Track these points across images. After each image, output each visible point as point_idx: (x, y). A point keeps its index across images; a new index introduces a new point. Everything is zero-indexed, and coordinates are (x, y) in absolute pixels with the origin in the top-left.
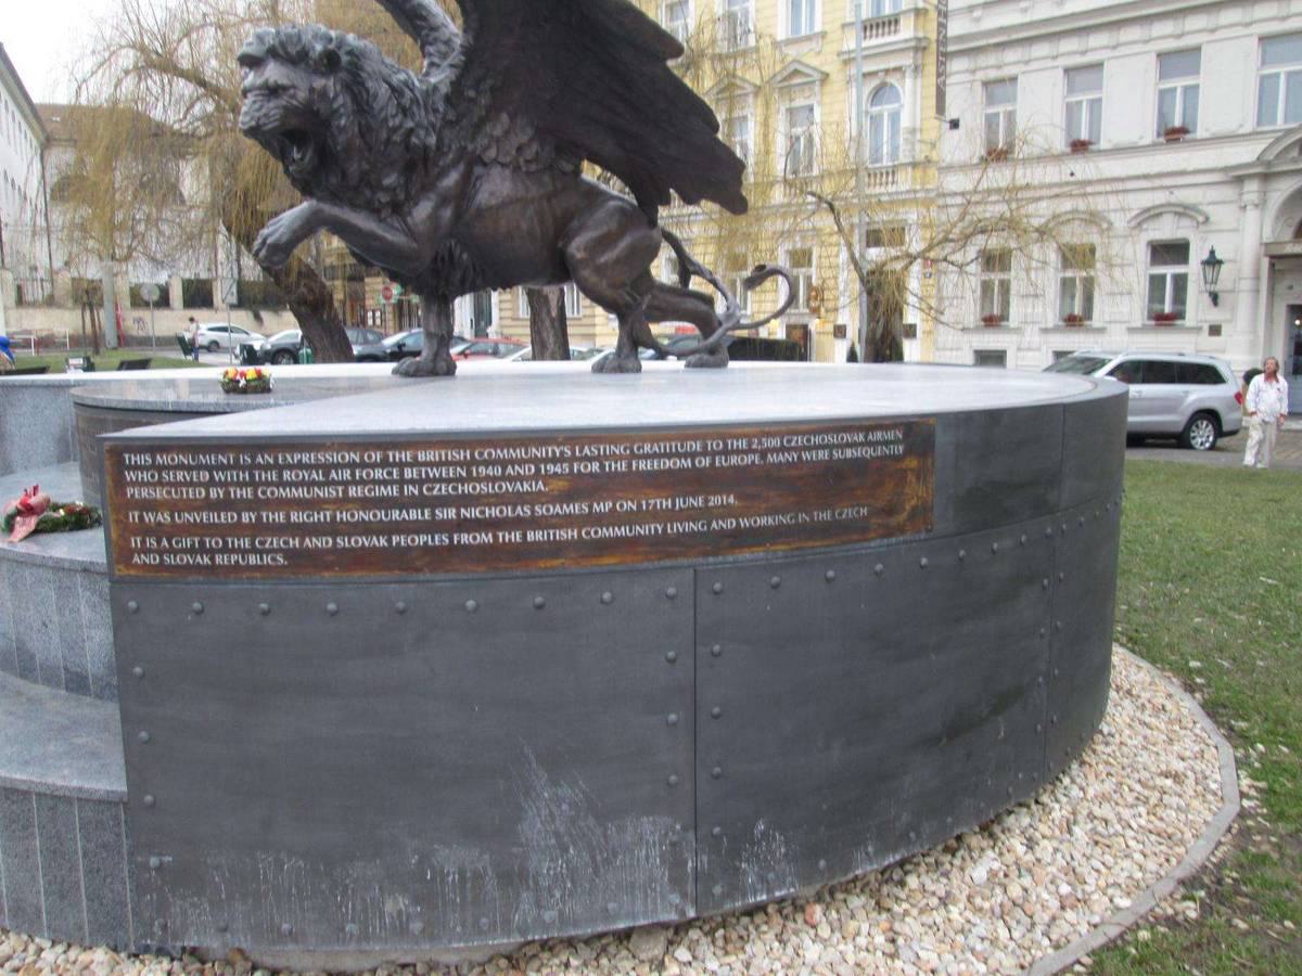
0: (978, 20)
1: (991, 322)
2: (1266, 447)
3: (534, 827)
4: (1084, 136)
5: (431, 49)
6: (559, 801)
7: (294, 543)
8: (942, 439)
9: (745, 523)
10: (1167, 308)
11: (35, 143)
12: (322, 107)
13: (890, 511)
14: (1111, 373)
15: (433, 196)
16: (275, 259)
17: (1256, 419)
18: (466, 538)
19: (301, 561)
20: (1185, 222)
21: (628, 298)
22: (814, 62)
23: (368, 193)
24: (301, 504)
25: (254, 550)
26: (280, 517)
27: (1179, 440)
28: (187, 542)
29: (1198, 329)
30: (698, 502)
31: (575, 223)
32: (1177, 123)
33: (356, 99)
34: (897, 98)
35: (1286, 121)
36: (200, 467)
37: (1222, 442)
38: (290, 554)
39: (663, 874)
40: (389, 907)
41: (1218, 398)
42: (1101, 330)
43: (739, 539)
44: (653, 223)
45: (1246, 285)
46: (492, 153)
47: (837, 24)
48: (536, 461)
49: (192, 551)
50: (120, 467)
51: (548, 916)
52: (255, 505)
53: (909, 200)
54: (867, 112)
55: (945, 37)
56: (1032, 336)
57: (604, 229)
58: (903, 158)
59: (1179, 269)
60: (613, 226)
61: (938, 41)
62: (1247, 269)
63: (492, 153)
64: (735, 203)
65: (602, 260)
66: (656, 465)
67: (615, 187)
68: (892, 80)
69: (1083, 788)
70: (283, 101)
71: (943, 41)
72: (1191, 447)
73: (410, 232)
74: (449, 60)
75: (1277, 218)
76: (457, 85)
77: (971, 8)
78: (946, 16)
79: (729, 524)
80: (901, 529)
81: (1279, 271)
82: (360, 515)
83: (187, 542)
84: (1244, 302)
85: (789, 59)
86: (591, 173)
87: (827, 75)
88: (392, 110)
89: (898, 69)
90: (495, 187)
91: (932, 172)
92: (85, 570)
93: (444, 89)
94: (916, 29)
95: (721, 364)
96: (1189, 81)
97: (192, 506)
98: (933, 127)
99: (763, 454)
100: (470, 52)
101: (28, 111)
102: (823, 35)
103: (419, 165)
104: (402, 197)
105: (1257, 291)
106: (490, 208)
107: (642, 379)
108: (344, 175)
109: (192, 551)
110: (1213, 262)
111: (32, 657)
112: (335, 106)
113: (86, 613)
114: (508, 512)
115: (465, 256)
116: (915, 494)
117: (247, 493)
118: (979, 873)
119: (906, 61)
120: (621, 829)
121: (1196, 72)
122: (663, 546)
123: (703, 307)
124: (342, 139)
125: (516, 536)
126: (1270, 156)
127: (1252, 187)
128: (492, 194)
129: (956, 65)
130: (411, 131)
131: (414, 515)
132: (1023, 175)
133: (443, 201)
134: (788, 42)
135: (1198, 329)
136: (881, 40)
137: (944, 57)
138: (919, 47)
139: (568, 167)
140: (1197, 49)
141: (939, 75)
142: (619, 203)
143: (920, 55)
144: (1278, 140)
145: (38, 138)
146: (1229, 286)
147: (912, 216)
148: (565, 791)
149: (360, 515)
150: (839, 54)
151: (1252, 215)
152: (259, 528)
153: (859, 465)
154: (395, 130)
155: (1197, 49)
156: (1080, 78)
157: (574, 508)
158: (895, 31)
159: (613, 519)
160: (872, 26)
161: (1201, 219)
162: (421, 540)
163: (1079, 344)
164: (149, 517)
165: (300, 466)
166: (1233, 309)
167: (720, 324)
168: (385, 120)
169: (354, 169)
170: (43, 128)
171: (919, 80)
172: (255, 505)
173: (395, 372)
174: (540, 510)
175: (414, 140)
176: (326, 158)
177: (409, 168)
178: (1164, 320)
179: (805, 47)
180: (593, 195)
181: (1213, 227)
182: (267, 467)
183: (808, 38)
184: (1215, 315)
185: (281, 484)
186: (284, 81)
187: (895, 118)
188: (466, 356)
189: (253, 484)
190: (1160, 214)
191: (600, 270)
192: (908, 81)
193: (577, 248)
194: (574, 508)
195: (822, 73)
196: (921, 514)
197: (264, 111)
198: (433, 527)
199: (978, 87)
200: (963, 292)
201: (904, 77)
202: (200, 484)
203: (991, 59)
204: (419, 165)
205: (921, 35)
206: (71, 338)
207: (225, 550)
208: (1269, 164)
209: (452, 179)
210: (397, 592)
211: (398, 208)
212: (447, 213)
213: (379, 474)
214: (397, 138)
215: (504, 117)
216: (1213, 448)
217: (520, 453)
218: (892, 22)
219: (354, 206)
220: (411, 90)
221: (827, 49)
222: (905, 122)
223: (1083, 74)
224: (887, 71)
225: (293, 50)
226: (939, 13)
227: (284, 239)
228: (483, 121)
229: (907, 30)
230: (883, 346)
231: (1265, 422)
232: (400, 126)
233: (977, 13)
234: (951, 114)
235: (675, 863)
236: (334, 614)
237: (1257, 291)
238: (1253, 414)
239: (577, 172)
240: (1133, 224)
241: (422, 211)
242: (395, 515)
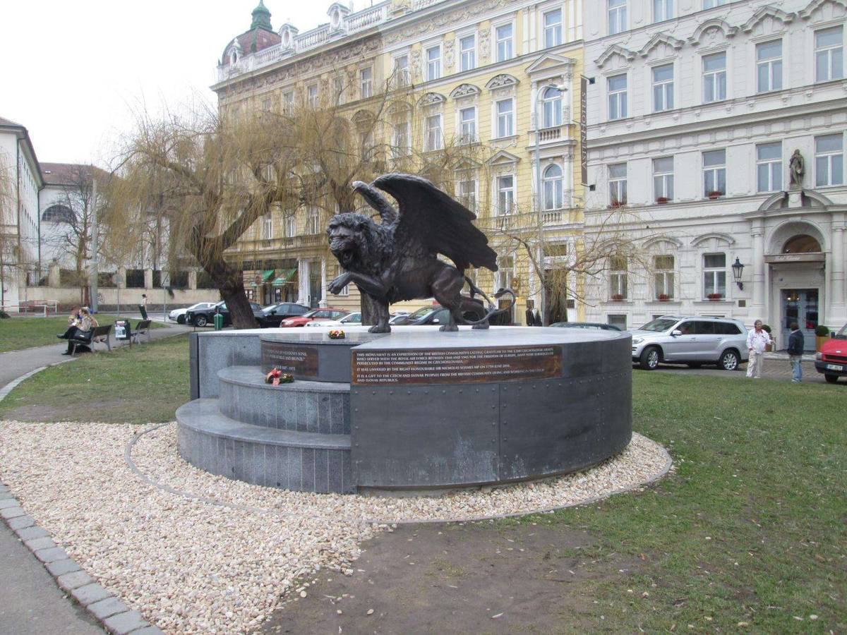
0: (603, 131)
1: (619, 299)
2: (758, 367)
3: (458, 453)
4: (665, 196)
5: (384, 215)
6: (464, 445)
8: (564, 351)
9: (512, 372)
10: (715, 291)
11: (36, 187)
12: (358, 242)
13: (550, 370)
14: (678, 328)
17: (752, 353)
18: (443, 375)
19: (401, 380)
20: (722, 243)
24: (402, 366)
25: (390, 378)
26: (397, 369)
27: (718, 364)
28: (372, 376)
29: (733, 303)
30: (500, 366)
31: (435, 276)
32: (715, 189)
33: (367, 238)
34: (559, 173)
35: (773, 189)
37: (741, 366)
38: (398, 378)
39: (491, 467)
40: (420, 474)
41: (736, 342)
42: (679, 304)
43: (511, 376)
44: (463, 275)
45: (757, 278)
46: (408, 253)
47: (526, 131)
48: (461, 355)
49: (374, 378)
50: (356, 357)
51: (461, 477)
52: (391, 366)
53: (567, 229)
54: (543, 180)
56: (639, 307)
57: (445, 279)
58: (565, 205)
59: (721, 269)
60: (449, 276)
62: (757, 270)
66: (490, 357)
67: (450, 262)
68: (556, 163)
69: (616, 465)
70: (346, 240)
71: (584, 142)
72: (724, 369)
73: (382, 282)
74: (395, 222)
75: (772, 241)
76: (397, 230)
77: (600, 125)
79: (508, 372)
80: (553, 376)
81: (775, 271)
82: (417, 369)
83: (372, 376)
84: (757, 288)
85: (498, 150)
86: (440, 257)
87: (520, 159)
88: (379, 242)
89: (560, 157)
90: (409, 264)
91: (581, 215)
92: (310, 392)
93: (393, 231)
94: (569, 136)
95: (487, 328)
96: (720, 167)
97: (374, 366)
98: (581, 190)
99: (517, 354)
100: (401, 219)
101: (34, 166)
102: (517, 137)
103: (386, 259)
105: (763, 282)
107: (459, 334)
108: (362, 263)
109: (374, 378)
110: (738, 265)
111: (284, 421)
113: (308, 405)
114: (454, 368)
116: (557, 366)
117: (389, 363)
118: (580, 481)
119: (565, 152)
120: (480, 454)
121: (724, 162)
122: (491, 377)
124: (364, 252)
125: (455, 374)
126: (766, 208)
127: (757, 224)
129: (592, 155)
131: (431, 369)
132: (628, 218)
133: (392, 271)
134: (497, 141)
135: (733, 303)
137: (585, 151)
138: (572, 145)
140: (723, 150)
141: (583, 161)
143: (572, 150)
144: (769, 199)
145: (37, 183)
146: (748, 279)
147: (571, 239)
148: (466, 443)
149: (417, 369)
150: (526, 148)
151: (758, 240)
152: (391, 372)
153: (541, 357)
155: (723, 150)
156: (661, 164)
157: (469, 367)
159: (479, 370)
160: (543, 133)
161: (731, 242)
162: (432, 375)
163: (665, 311)
164: (363, 370)
165: (403, 356)
166: (751, 293)
167: (487, 312)
169: (365, 262)
170: (42, 179)
172: (391, 366)
173: (371, 331)
174: (462, 368)
176: (357, 257)
177: (383, 260)
178: (715, 298)
179: (507, 144)
180: (442, 264)
181: (739, 246)
182: (394, 357)
183: (509, 139)
184: (741, 295)
186: (346, 234)
187: (559, 183)
188: (313, 318)
189: (391, 361)
190: (708, 239)
191: (444, 293)
192: (566, 164)
193: (436, 285)
194: (469, 367)
195: (517, 158)
196: (559, 371)
198: (435, 372)
199: (606, 168)
200: (600, 287)
201: (563, 162)
203: (609, 153)
204: (386, 259)
205: (572, 138)
206: (58, 305)
207: (382, 378)
208: (765, 212)
209: (395, 264)
210: (425, 389)
211: (377, 274)
212: (394, 275)
213: (422, 358)
214: (380, 251)
215: (412, 240)
216: (736, 369)
217: (457, 353)
218: (556, 131)
219: (363, 273)
221: (520, 144)
222: (565, 186)
223: (662, 162)
224: (554, 158)
225: (350, 224)
226: (582, 128)
229: (564, 136)
230: (556, 315)
231: (757, 354)
233: (603, 128)
234: (590, 182)
235: (495, 465)
237: (763, 282)
238: (751, 349)
240: (694, 244)
241: (386, 274)
242: (426, 369)
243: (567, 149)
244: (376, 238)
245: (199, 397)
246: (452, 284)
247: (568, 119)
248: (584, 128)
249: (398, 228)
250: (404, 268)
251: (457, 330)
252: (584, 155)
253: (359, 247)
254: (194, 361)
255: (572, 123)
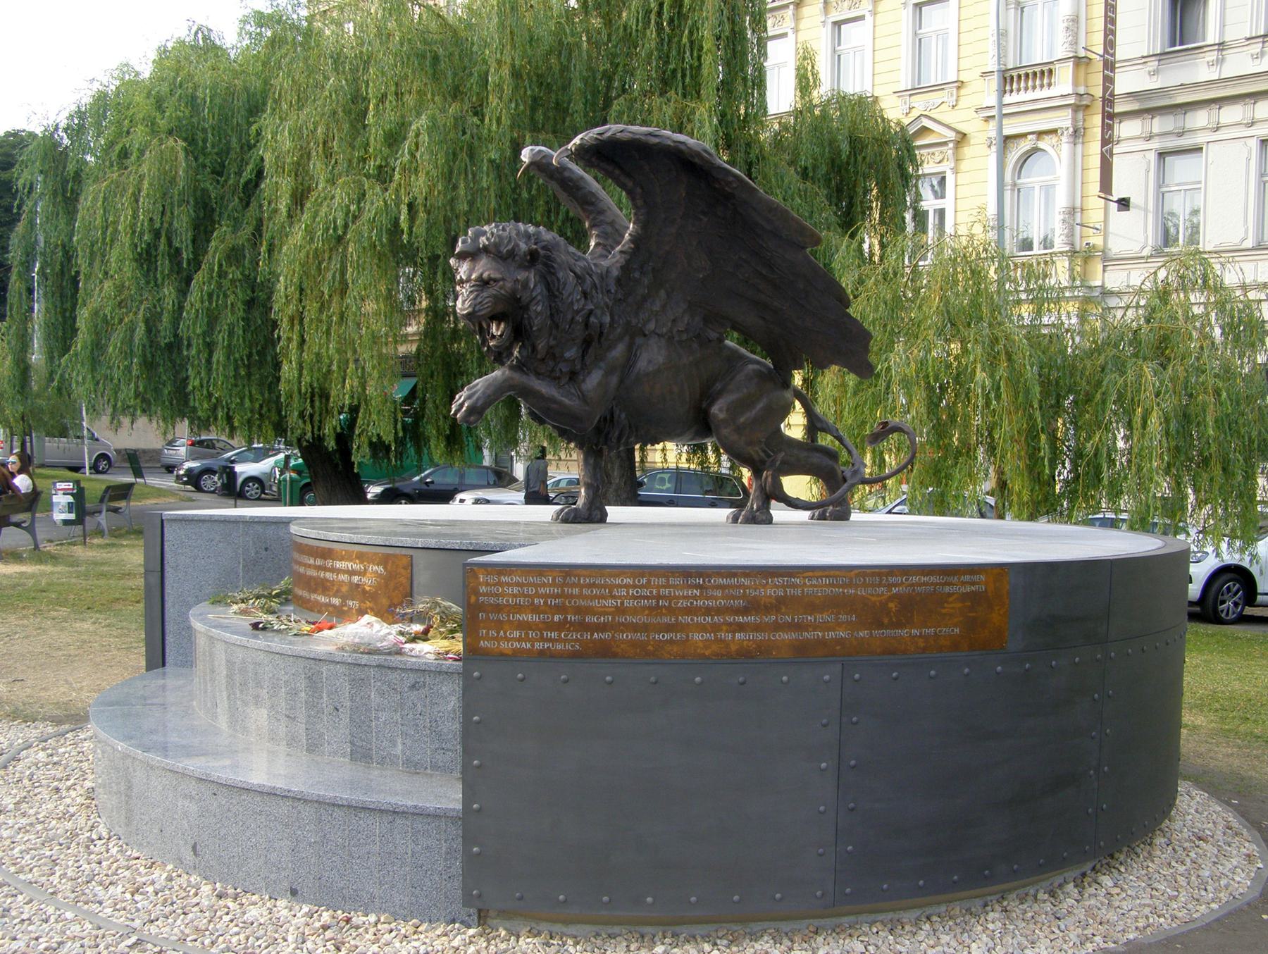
7: (587, 636)
12: (525, 297)
15: (602, 364)
16: (472, 418)
21: (762, 454)
22: (948, 118)
23: (551, 363)
31: (718, 386)
33: (548, 287)
36: (529, 585)
46: (652, 326)
49: (519, 640)
55: (1112, 95)
61: (1103, 97)
63: (652, 326)
64: (864, 370)
65: (742, 420)
70: (491, 291)
76: (626, 268)
78: (1113, 69)
90: (652, 356)
94: (1076, 83)
104: (579, 367)
106: (647, 374)
109: (519, 640)
112: (534, 294)
115: (623, 416)
123: (827, 461)
124: (537, 322)
128: (650, 362)
130: (591, 312)
133: (608, 373)
136: (1030, 95)
139: (713, 335)
142: (756, 367)
154: (578, 312)
158: (1050, 85)
167: (845, 480)
168: (572, 303)
169: (541, 345)
171: (1079, 147)
175: (592, 319)
180: (734, 359)
183: (938, 87)
185: (581, 596)
191: (739, 430)
193: (718, 410)
195: (958, 132)
197: (479, 300)
202: (529, 596)
204: (593, 341)
205: (1082, 90)
209: (618, 351)
211: (573, 376)
212: (614, 380)
214: (579, 319)
215: (662, 293)
219: (538, 375)
220: (590, 276)
224: (1040, 134)
227: (480, 403)
228: (645, 299)
232: (583, 309)
236: (610, 683)
239: (721, 340)
241: (592, 381)
243: (1068, 113)
244: (569, 288)
245: (164, 665)
246: (760, 405)
247: (1075, 43)
248: (1110, 66)
249: (628, 262)
250: (642, 364)
251: (769, 520)
252: (1107, 128)
253: (526, 308)
254: (155, 579)
255: (1082, 53)
